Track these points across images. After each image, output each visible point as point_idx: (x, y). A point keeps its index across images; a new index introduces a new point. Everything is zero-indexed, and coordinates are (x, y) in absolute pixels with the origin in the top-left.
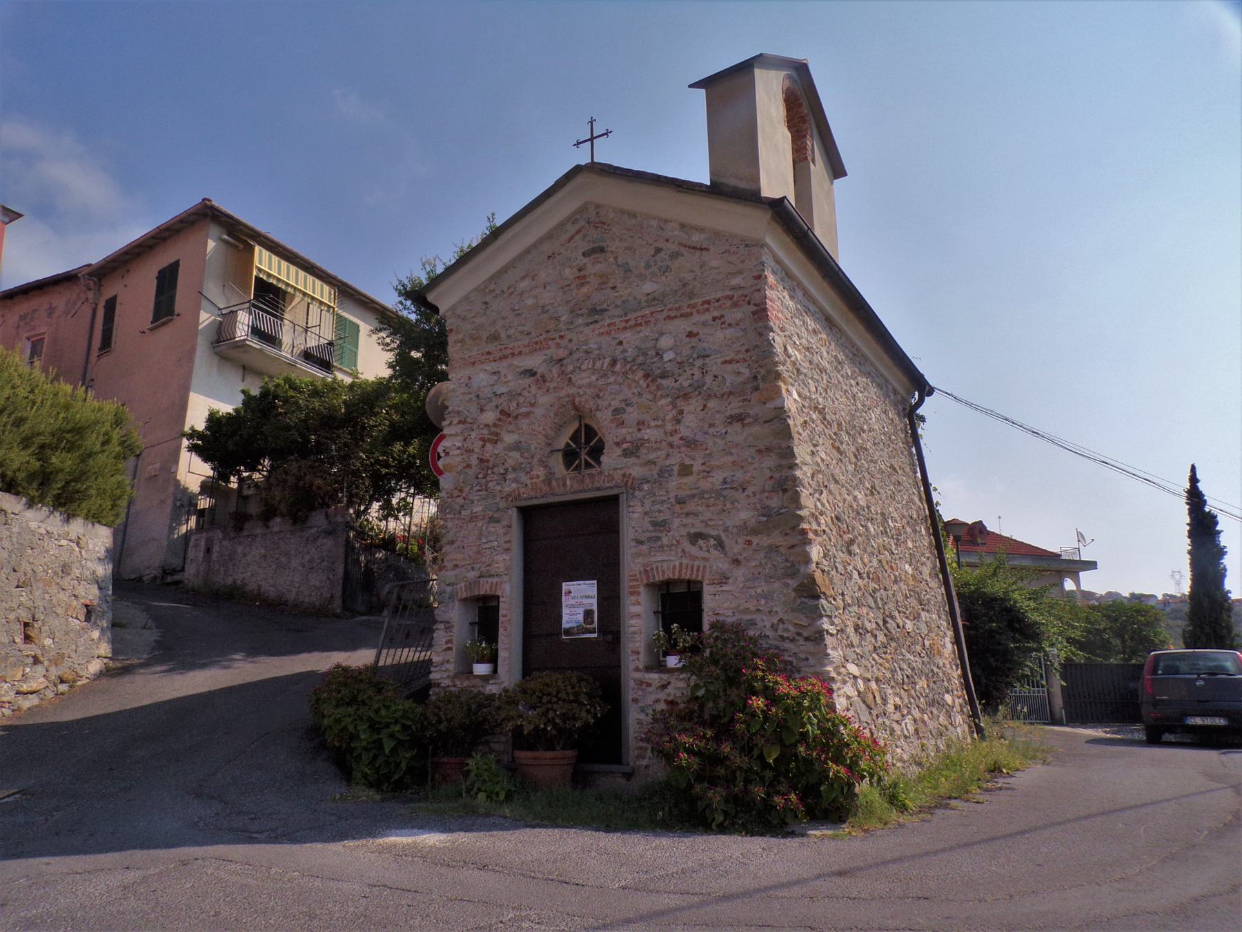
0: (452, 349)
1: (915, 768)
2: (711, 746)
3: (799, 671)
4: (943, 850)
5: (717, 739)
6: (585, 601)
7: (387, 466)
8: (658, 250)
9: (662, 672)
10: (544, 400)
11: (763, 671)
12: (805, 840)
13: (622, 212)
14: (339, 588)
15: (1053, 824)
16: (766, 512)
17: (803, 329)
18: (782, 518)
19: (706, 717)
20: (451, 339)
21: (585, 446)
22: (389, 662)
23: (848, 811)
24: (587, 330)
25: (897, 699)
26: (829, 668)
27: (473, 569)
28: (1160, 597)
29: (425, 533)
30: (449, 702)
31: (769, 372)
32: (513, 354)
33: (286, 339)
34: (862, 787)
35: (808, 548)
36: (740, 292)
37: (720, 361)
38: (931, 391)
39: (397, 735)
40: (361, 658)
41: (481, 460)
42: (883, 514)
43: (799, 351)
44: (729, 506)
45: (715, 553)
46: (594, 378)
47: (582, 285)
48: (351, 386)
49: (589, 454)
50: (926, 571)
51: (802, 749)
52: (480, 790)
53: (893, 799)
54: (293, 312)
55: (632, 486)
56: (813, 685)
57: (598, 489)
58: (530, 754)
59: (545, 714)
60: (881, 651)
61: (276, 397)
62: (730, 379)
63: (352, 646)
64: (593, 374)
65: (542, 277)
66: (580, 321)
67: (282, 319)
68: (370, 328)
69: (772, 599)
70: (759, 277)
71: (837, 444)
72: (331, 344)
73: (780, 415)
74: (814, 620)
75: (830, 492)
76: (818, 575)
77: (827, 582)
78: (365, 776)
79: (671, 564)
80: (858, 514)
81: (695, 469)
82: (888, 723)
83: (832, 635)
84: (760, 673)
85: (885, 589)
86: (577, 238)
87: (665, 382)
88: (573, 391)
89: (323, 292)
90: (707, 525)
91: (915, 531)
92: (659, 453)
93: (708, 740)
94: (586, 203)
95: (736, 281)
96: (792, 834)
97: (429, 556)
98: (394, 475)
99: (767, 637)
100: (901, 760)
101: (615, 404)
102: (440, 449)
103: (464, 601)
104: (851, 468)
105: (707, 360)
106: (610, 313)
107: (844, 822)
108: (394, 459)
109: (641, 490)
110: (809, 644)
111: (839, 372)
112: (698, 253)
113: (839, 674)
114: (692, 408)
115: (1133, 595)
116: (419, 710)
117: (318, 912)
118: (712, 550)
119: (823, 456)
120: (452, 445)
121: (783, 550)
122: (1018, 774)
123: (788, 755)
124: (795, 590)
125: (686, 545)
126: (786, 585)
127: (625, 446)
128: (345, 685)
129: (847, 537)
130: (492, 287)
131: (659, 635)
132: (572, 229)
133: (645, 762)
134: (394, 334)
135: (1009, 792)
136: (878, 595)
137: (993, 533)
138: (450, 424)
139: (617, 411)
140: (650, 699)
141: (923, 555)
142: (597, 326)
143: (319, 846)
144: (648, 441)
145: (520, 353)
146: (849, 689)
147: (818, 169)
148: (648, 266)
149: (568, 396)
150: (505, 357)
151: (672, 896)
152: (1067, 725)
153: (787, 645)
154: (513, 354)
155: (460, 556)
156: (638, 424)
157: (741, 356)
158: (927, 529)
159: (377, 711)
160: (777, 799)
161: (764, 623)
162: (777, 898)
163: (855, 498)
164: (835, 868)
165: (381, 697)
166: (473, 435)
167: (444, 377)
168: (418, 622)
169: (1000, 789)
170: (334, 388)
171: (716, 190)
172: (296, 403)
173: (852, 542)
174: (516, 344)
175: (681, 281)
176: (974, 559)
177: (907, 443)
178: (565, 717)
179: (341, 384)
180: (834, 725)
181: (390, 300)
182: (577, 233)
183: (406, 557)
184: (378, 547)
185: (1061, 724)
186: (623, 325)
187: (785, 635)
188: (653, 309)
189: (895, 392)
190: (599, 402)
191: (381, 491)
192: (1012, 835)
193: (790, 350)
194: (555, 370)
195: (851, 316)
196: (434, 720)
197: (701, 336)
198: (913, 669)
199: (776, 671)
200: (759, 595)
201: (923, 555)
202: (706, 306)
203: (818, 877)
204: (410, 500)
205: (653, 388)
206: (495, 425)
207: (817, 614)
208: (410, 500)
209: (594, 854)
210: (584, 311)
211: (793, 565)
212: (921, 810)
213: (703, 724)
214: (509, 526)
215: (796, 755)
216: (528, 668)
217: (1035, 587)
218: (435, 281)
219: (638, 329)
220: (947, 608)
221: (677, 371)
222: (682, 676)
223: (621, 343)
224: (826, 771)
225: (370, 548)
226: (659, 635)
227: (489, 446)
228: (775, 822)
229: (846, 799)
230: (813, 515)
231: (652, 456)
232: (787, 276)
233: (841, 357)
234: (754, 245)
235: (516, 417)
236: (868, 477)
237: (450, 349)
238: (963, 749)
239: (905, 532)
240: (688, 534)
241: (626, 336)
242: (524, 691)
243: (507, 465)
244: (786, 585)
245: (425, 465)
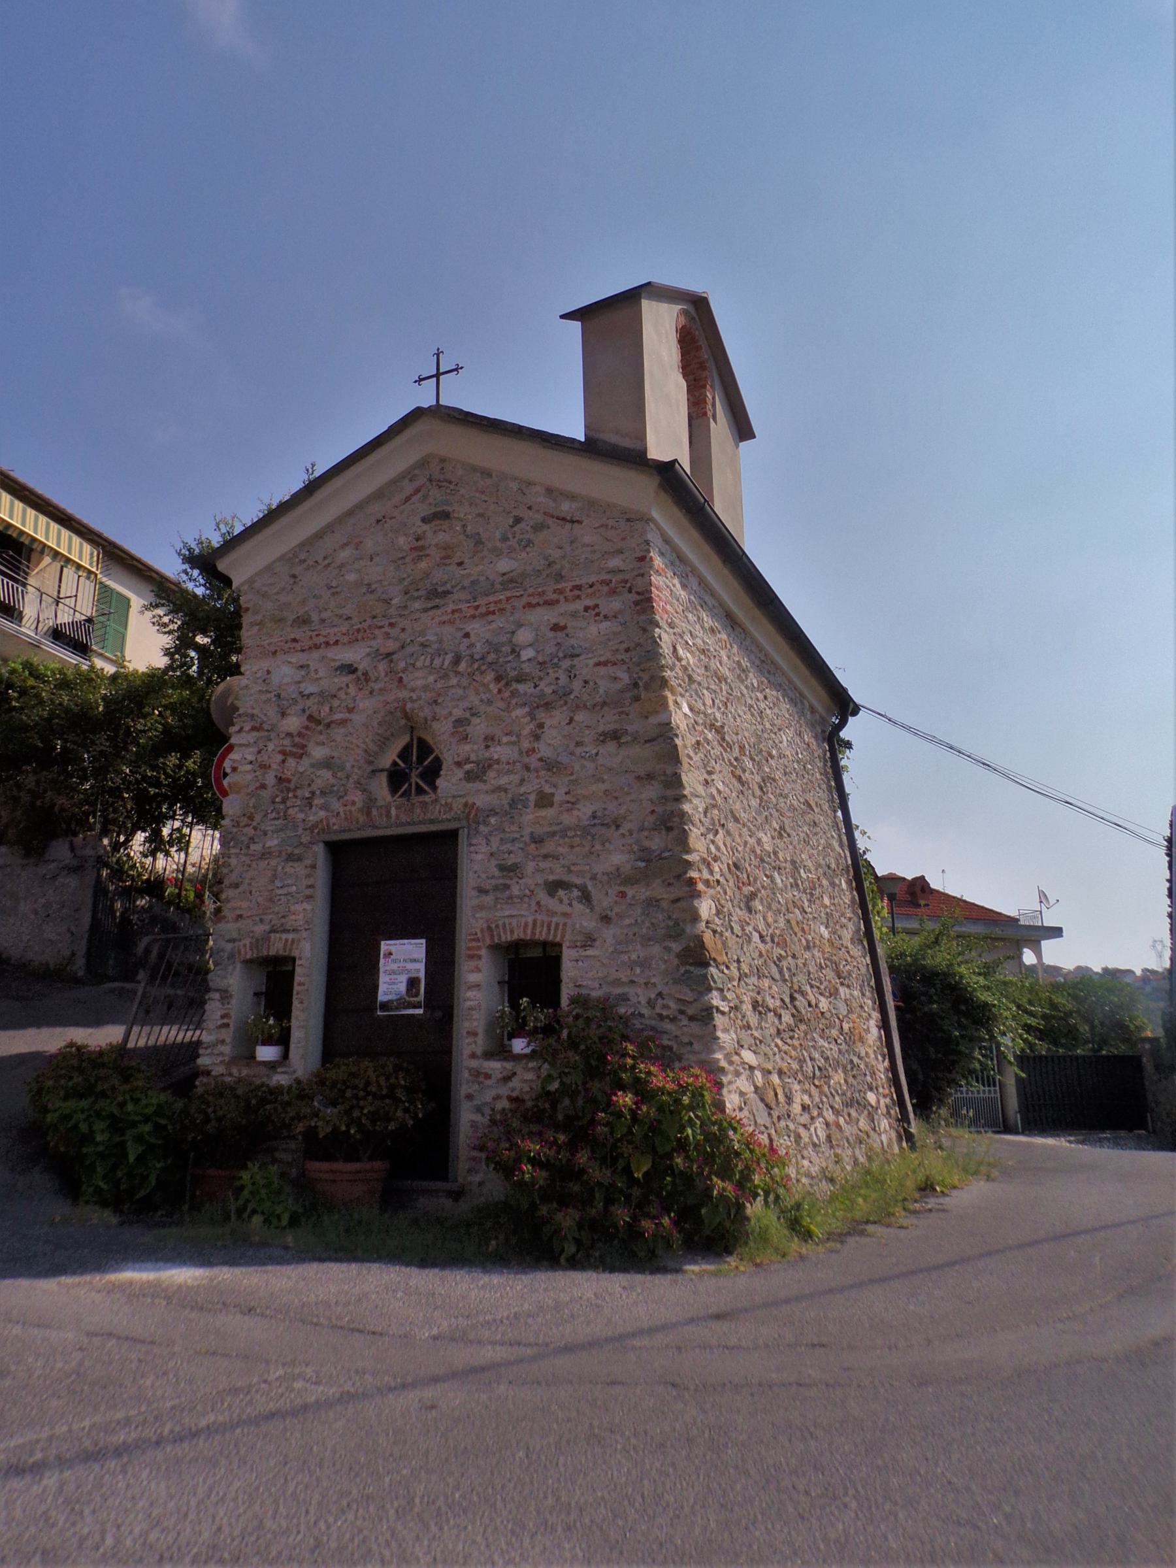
0: (248, 635)
1: (825, 1186)
2: (564, 1155)
3: (680, 1059)
4: (851, 1287)
5: (572, 1146)
6: (410, 966)
7: (157, 784)
8: (518, 520)
9: (505, 1059)
10: (366, 704)
11: (633, 1058)
12: (679, 1277)
13: (474, 469)
14: (84, 943)
15: (989, 1254)
16: (646, 855)
17: (698, 627)
18: (665, 865)
19: (560, 1117)
20: (246, 620)
21: (416, 767)
22: (141, 1043)
23: (736, 1239)
25: (806, 1098)
26: (719, 1056)
27: (261, 921)
28: (1138, 973)
29: (205, 876)
30: (221, 1095)
31: (652, 678)
32: (327, 644)
33: (30, 611)
34: (755, 1209)
35: (696, 903)
36: (620, 577)
37: (591, 662)
38: (856, 710)
39: (147, 1137)
40: (104, 1037)
41: (280, 780)
42: (793, 862)
43: (691, 652)
44: (598, 847)
45: (579, 907)
46: (431, 679)
47: (420, 558)
48: (114, 678)
49: (422, 776)
50: (847, 935)
51: (679, 1160)
52: (254, 1212)
53: (796, 1226)
54: (42, 575)
55: (474, 816)
56: (697, 1077)
57: (432, 822)
58: (324, 1166)
59: (348, 1112)
60: (786, 1036)
61: (10, 685)
62: (604, 686)
63: (96, 1020)
64: (430, 673)
65: (369, 545)
66: (417, 605)
67: (24, 585)
68: (143, 602)
69: (649, 967)
70: (642, 559)
71: (739, 772)
72: (89, 620)
73: (666, 733)
74: (701, 994)
75: (728, 833)
76: (708, 937)
77: (720, 946)
78: (98, 1191)
79: (520, 920)
80: (762, 860)
81: (557, 799)
82: (792, 1126)
83: (723, 1013)
84: (630, 1061)
85: (794, 956)
86: (415, 498)
87: (521, 687)
88: (404, 694)
89: (82, 552)
90: (570, 871)
91: (833, 884)
92: (512, 777)
93: (560, 1147)
94: (428, 456)
95: (615, 562)
96: (663, 1270)
97: (209, 906)
98: (165, 798)
99: (641, 1015)
100: (808, 1175)
101: (458, 713)
102: (227, 765)
103: (248, 963)
104: (754, 803)
105: (576, 660)
106: (456, 596)
107: (730, 1253)
108: (167, 776)
109: (486, 824)
110: (693, 1024)
111: (742, 681)
112: (569, 525)
113: (731, 1063)
114: (555, 721)
115: (1106, 970)
116: (179, 1105)
117: (13, 1368)
118: (575, 903)
119: (721, 786)
120: (241, 759)
121: (664, 904)
122: (955, 1193)
123: (662, 1167)
124: (678, 956)
125: (542, 895)
126: (668, 949)
127: (468, 767)
128: (81, 1070)
129: (747, 890)
131: (503, 1012)
132: (409, 488)
133: (478, 1178)
134: (173, 612)
135: (941, 1215)
136: (784, 964)
137: (937, 891)
139: (459, 722)
140: (488, 1096)
141: (843, 915)
142: (439, 612)
143: (24, 1283)
144: (498, 762)
146: (743, 1083)
147: (720, 428)
148: (505, 539)
149: (397, 700)
150: (317, 647)
151: (498, 1348)
152: (1023, 1133)
153: (667, 1026)
154: (327, 644)
155: (245, 904)
156: (486, 739)
157: (620, 657)
158: (849, 882)
159: (122, 1105)
160: (647, 1225)
161: (640, 997)
162: (634, 1348)
163: (759, 841)
164: (713, 1310)
165: (127, 1087)
166: (271, 746)
167: (235, 670)
168: (187, 990)
169: (930, 1210)
170: (91, 679)
171: (592, 448)
172: (37, 696)
173: (753, 896)
175: (546, 559)
176: (914, 925)
177: (825, 774)
178: (374, 1117)
179: (99, 674)
180: (721, 1129)
181: (171, 567)
182: (417, 491)
183: (178, 907)
184: (141, 892)
185: (1017, 1133)
186: (472, 612)
187: (665, 1013)
188: (508, 593)
189: (813, 710)
190: (437, 709)
191: (149, 818)
192: (937, 1267)
193: (681, 652)
194: (382, 667)
195: (757, 612)
196: (199, 1118)
197: (569, 630)
198: (827, 1059)
199: (650, 1058)
200: (634, 962)
201: (843, 915)
202: (577, 592)
203: (691, 1321)
204: (186, 831)
206: (300, 734)
207: (705, 985)
208: (186, 831)
209: (400, 1294)
210: (421, 593)
211: (677, 924)
212: (830, 1236)
213: (557, 1127)
214: (313, 867)
215: (671, 1167)
216: (329, 1053)
217: (987, 958)
218: (232, 543)
219: (491, 618)
220: (873, 983)
222: (530, 1065)
223: (467, 635)
224: (710, 1189)
225: (128, 893)
226: (503, 1012)
227: (291, 762)
228: (642, 1254)
229: (733, 1222)
230: (704, 860)
231: (503, 781)
232: (678, 560)
233: (745, 663)
234: (636, 519)
235: (328, 726)
236: (775, 814)
237: (244, 633)
238: (888, 1162)
239: (821, 886)
241: (476, 628)
242: (322, 1082)
243: (314, 787)
244: (668, 949)
245: (208, 786)
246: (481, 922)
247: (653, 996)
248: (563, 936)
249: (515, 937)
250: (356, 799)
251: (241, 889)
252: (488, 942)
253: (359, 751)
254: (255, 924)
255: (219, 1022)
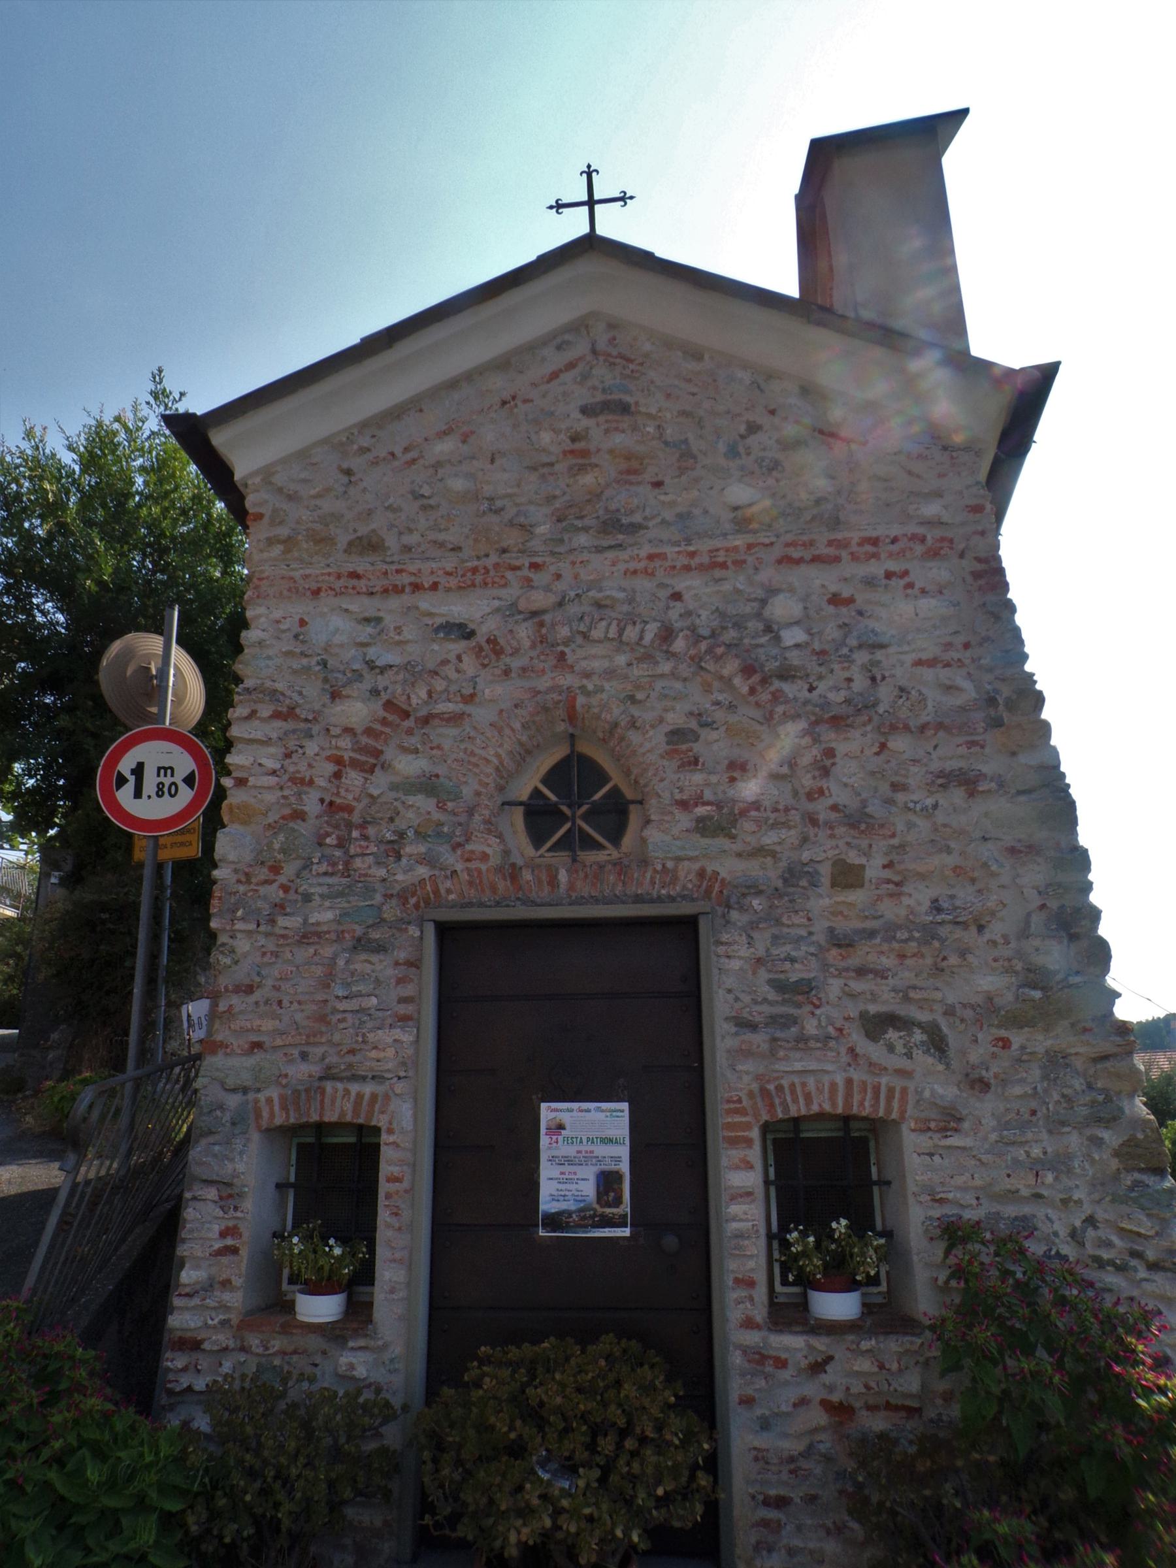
6: (601, 1150)
10: (498, 692)
21: (579, 799)
24: (600, 563)
27: (304, 1056)
36: (938, 533)
37: (909, 659)
44: (953, 960)
45: (924, 1061)
47: (582, 469)
57: (638, 899)
69: (1070, 1171)
79: (819, 1082)
86: (567, 377)
87: (789, 689)
88: (568, 680)
90: (906, 999)
92: (783, 834)
95: (931, 509)
101: (676, 719)
105: (879, 655)
118: (918, 1054)
124: (1116, 1154)
125: (857, 1038)
126: (1097, 1142)
127: (701, 811)
130: (365, 441)
132: (554, 360)
138: (253, 714)
139: (677, 735)
142: (624, 555)
145: (435, 587)
150: (398, 590)
154: (417, 587)
155: (268, 1025)
157: (955, 655)
166: (312, 748)
174: (426, 567)
182: (571, 366)
186: (684, 560)
187: (1106, 1255)
188: (750, 539)
190: (635, 711)
200: (1037, 1161)
202: (869, 548)
205: (765, 697)
206: (369, 731)
211: (1108, 1100)
219: (718, 573)
221: (813, 667)
223: (677, 596)
227: (353, 778)
231: (769, 839)
240: (863, 1015)
241: (692, 585)
246: (746, 1079)
247: (1078, 1223)
248: (903, 1112)
249: (815, 1108)
250: (488, 850)
251: (257, 995)
252: (765, 1117)
253: (490, 770)
254: (291, 1061)
255: (217, 1245)
